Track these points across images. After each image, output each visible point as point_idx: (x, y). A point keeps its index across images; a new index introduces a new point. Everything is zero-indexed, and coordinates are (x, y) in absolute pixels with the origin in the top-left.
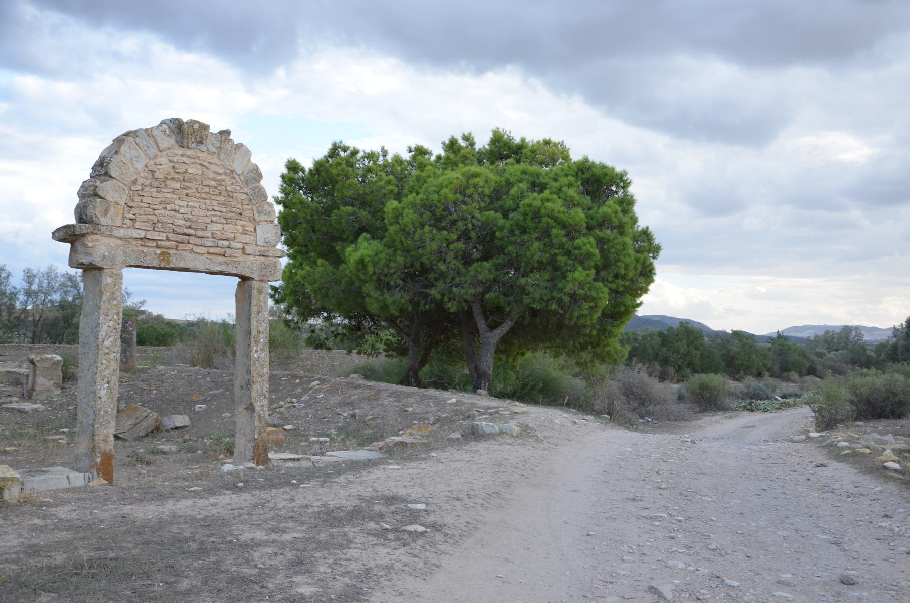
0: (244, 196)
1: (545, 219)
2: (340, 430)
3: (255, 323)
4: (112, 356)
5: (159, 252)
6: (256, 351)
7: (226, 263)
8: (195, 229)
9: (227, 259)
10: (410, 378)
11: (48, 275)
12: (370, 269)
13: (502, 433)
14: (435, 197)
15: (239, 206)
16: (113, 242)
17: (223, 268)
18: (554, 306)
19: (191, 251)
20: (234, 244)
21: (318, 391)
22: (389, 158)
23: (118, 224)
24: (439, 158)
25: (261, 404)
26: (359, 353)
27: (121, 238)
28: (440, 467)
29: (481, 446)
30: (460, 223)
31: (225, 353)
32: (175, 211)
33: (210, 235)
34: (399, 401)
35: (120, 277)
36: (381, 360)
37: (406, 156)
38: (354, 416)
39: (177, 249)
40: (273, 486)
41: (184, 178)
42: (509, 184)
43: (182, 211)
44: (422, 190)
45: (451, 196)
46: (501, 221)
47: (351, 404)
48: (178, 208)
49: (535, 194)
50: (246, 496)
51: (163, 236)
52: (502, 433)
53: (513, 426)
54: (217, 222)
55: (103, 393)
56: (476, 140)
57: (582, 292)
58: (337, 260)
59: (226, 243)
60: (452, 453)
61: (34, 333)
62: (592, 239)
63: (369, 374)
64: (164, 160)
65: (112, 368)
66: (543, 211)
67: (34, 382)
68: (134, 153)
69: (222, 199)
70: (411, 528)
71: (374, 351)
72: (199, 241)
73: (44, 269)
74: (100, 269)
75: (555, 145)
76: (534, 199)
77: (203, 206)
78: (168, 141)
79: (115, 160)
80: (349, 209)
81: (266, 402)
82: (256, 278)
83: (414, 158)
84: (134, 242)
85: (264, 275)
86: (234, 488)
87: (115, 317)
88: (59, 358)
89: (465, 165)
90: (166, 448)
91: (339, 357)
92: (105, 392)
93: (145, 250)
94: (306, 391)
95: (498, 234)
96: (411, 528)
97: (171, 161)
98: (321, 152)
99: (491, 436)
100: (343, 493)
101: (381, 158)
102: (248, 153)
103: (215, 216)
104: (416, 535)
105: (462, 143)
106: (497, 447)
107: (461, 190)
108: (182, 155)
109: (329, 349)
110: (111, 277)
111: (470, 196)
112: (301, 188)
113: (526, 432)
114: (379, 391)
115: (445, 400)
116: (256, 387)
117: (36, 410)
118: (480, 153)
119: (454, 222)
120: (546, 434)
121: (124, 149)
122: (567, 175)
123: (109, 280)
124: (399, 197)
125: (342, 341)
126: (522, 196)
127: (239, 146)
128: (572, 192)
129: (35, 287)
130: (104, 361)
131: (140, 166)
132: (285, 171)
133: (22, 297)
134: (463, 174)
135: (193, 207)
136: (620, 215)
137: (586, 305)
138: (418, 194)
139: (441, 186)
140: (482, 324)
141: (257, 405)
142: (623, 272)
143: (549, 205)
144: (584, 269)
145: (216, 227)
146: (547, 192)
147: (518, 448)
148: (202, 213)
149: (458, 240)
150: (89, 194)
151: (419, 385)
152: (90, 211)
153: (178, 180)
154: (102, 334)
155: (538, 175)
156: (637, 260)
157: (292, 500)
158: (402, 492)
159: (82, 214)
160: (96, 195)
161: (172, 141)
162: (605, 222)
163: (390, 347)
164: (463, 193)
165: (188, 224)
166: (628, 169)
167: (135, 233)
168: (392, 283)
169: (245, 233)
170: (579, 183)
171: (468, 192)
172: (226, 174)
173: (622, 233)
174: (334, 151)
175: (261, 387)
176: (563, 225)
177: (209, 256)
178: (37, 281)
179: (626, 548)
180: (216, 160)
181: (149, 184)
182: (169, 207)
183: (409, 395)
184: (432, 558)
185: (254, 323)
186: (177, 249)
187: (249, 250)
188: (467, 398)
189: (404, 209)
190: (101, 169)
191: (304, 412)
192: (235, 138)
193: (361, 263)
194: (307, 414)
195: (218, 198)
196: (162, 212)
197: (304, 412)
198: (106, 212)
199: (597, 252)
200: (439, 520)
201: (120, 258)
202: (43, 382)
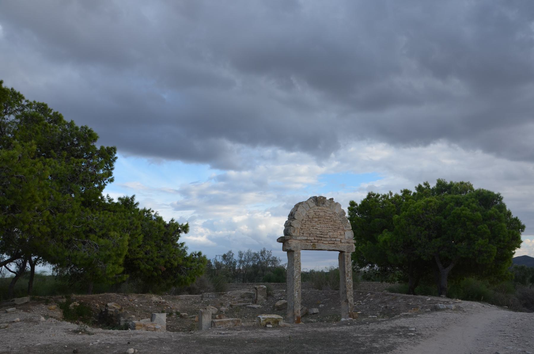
1: (462, 219)
2: (381, 313)
10: (411, 291)
11: (248, 253)
12: (389, 244)
13: (447, 308)
14: (414, 212)
16: (297, 242)
17: (334, 248)
18: (471, 255)
19: (323, 243)
20: (337, 239)
21: (370, 298)
22: (393, 196)
24: (415, 194)
25: (351, 299)
26: (386, 282)
28: (421, 319)
29: (438, 313)
30: (426, 222)
31: (326, 284)
34: (405, 300)
35: (300, 254)
36: (397, 284)
37: (400, 194)
38: (386, 307)
39: (318, 242)
40: (360, 324)
41: (319, 217)
42: (446, 204)
44: (408, 210)
45: (421, 211)
46: (443, 220)
47: (385, 302)
49: (458, 208)
50: (351, 327)
51: (313, 238)
52: (447, 308)
53: (453, 306)
55: (296, 295)
56: (430, 184)
57: (483, 249)
58: (374, 241)
60: (427, 315)
61: (243, 279)
62: (486, 225)
63: (392, 290)
64: (312, 211)
66: (462, 215)
67: (257, 297)
68: (302, 210)
69: (332, 223)
70: (409, 334)
71: (393, 281)
73: (246, 251)
74: (293, 251)
75: (466, 184)
76: (457, 210)
78: (313, 205)
79: (296, 213)
80: (378, 219)
81: (352, 299)
83: (404, 195)
86: (347, 325)
88: (265, 287)
89: (426, 197)
90: (312, 320)
91: (377, 284)
94: (365, 298)
95: (443, 226)
96: (409, 334)
98: (365, 196)
99: (443, 310)
100: (385, 326)
101: (390, 196)
102: (340, 206)
104: (411, 336)
105: (424, 186)
106: (445, 313)
107: (425, 208)
109: (373, 281)
111: (429, 211)
112: (356, 212)
113: (458, 309)
114: (396, 297)
115: (426, 300)
116: (348, 293)
117: (259, 308)
118: (433, 189)
119: (423, 222)
120: (468, 310)
121: (299, 209)
122: (472, 198)
123: (296, 255)
124: (398, 213)
125: (378, 277)
126: (452, 208)
127: (337, 203)
128: (474, 205)
129: (243, 259)
131: (304, 214)
132: (349, 206)
133: (238, 264)
134: (425, 202)
136: (499, 213)
137: (485, 255)
138: (406, 211)
139: (416, 208)
140: (440, 266)
141: (349, 300)
142: (502, 239)
143: (464, 212)
144: (483, 239)
145: (331, 234)
146: (463, 206)
147: (454, 314)
148: (326, 229)
149: (425, 229)
150: (288, 225)
151: (414, 294)
152: (289, 231)
153: (317, 218)
154: (295, 274)
155: (459, 198)
156: (509, 233)
157: (368, 328)
158: (407, 326)
159: (286, 232)
160: (291, 226)
161: (314, 204)
162: (491, 217)
163: (400, 279)
164: (426, 210)
166: (500, 192)
168: (399, 249)
169: (341, 235)
170: (477, 201)
171: (428, 209)
173: (500, 221)
174: (370, 195)
175: (350, 293)
176: (472, 220)
178: (244, 256)
179: (491, 343)
180: (329, 209)
181: (307, 220)
183: (409, 298)
184: (417, 341)
185: (346, 268)
186: (318, 242)
187: (343, 241)
188: (435, 298)
189: (401, 218)
190: (291, 216)
191: (365, 306)
192: (335, 201)
193: (385, 242)
194: (366, 307)
197: (365, 306)
198: (294, 231)
199: (489, 231)
200: (420, 333)
201: (299, 247)
202: (260, 297)
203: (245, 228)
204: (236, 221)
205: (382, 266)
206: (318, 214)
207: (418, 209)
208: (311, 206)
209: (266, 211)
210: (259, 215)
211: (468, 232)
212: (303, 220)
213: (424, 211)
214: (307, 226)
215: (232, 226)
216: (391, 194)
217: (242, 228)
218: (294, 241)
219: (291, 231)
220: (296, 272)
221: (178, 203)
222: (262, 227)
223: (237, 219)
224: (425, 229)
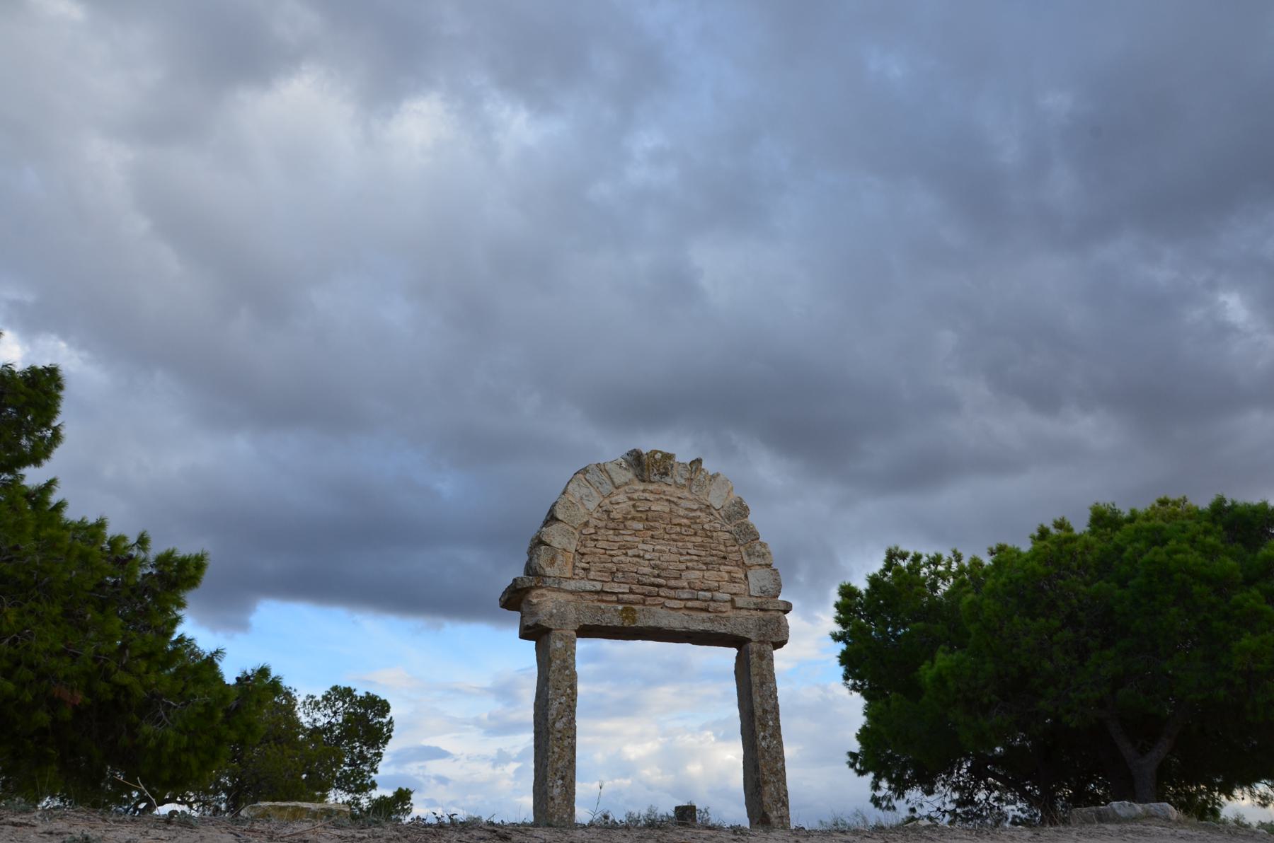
0: (727, 536)
3: (759, 700)
4: (566, 743)
5: (620, 607)
6: (764, 738)
7: (712, 621)
8: (666, 578)
9: (712, 615)
12: (951, 683)
15: (722, 547)
16: (562, 597)
17: (698, 623)
19: (663, 606)
20: (718, 595)
22: (966, 562)
23: (568, 575)
32: (638, 556)
33: (685, 584)
41: (648, 518)
42: (1120, 550)
43: (647, 556)
46: (1118, 592)
48: (641, 553)
55: (556, 791)
58: (913, 690)
59: (708, 595)
64: (621, 497)
65: (567, 758)
68: (585, 491)
69: (699, 539)
72: (672, 593)
74: (548, 631)
77: (674, 549)
82: (753, 639)
84: (588, 597)
85: (764, 635)
87: (569, 691)
92: (559, 790)
93: (603, 606)
97: (630, 499)
103: (691, 561)
108: (644, 491)
123: (559, 644)
130: (556, 749)
131: (592, 506)
135: (661, 551)
143: (1179, 556)
148: (673, 557)
153: (640, 520)
161: (630, 475)
165: (656, 572)
167: (589, 586)
169: (732, 580)
170: (1220, 528)
172: (701, 510)
177: (687, 612)
180: (686, 494)
182: (630, 552)
187: (740, 602)
193: (940, 680)
195: (693, 539)
196: (623, 558)
198: (552, 561)
203: (651, 774)
204: (633, 757)
205: (948, 767)
206: (643, 506)
209: (703, 728)
210: (688, 740)
212: (586, 524)
214: (601, 544)
215: (626, 768)
217: (647, 772)
218: (554, 595)
219: (542, 559)
220: (555, 705)
221: (491, 717)
222: (694, 769)
223: (633, 752)
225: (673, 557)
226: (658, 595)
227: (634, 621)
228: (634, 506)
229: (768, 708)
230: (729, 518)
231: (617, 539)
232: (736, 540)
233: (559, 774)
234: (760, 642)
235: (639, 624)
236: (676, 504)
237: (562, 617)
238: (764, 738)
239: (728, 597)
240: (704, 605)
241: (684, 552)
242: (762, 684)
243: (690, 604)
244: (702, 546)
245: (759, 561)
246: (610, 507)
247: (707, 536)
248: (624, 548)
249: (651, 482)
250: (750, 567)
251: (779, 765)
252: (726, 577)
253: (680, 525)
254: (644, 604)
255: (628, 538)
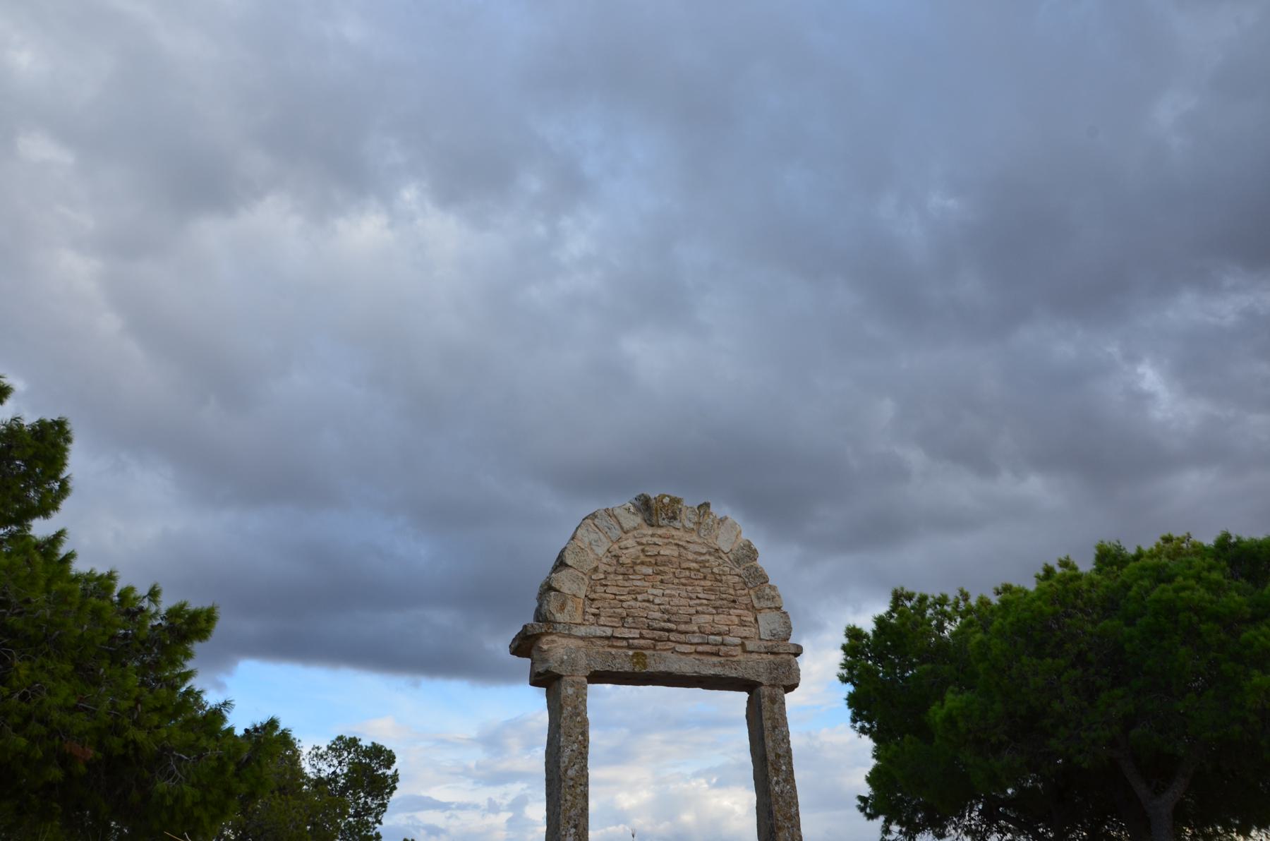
0: (737, 579)
3: (771, 744)
4: (578, 791)
5: (631, 653)
6: (778, 783)
7: (722, 665)
9: (722, 660)
15: (731, 591)
16: (573, 643)
19: (674, 651)
20: (728, 639)
23: (579, 621)
27: (582, 638)
32: (648, 601)
33: (696, 628)
41: (658, 562)
43: (657, 601)
48: (651, 598)
54: (703, 613)
58: (924, 732)
59: (719, 638)
64: (630, 542)
68: (593, 536)
69: (708, 583)
72: (682, 638)
74: (559, 677)
76: (1164, 590)
77: (684, 594)
82: (765, 682)
85: (775, 679)
87: (580, 738)
93: (613, 651)
95: (1127, 646)
97: (639, 544)
101: (962, 604)
103: (701, 605)
108: (652, 535)
110: (572, 686)
123: (570, 691)
128: (1215, 576)
130: (568, 797)
131: (601, 551)
135: (671, 596)
148: (683, 602)
153: (650, 565)
161: (638, 520)
165: (666, 617)
167: (599, 631)
169: (743, 624)
170: (1223, 563)
172: (710, 554)
176: (1216, 617)
177: (697, 657)
180: (694, 537)
182: (640, 597)
187: (750, 646)
193: (950, 720)
195: (702, 583)
196: (632, 603)
198: (562, 608)
206: (652, 551)
207: (1039, 603)
208: (626, 526)
211: (1212, 655)
212: (596, 570)
213: (1057, 607)
216: (965, 597)
218: (565, 641)
219: (552, 604)
220: (567, 752)
224: (1073, 666)
225: (683, 602)
226: (669, 640)
227: (645, 666)
228: (643, 551)
229: (780, 752)
230: (737, 561)
231: (626, 584)
232: (745, 583)
233: (572, 822)
234: (771, 685)
235: (651, 670)
236: (684, 548)
237: (573, 663)
238: (778, 783)
239: (738, 641)
240: (714, 649)
241: (694, 596)
242: (774, 728)
243: (700, 648)
244: (711, 590)
245: (769, 604)
246: (619, 552)
247: (717, 580)
248: (634, 592)
249: (659, 526)
250: (760, 610)
251: (793, 810)
252: (736, 620)
253: (689, 569)
254: (654, 649)
255: (638, 583)
